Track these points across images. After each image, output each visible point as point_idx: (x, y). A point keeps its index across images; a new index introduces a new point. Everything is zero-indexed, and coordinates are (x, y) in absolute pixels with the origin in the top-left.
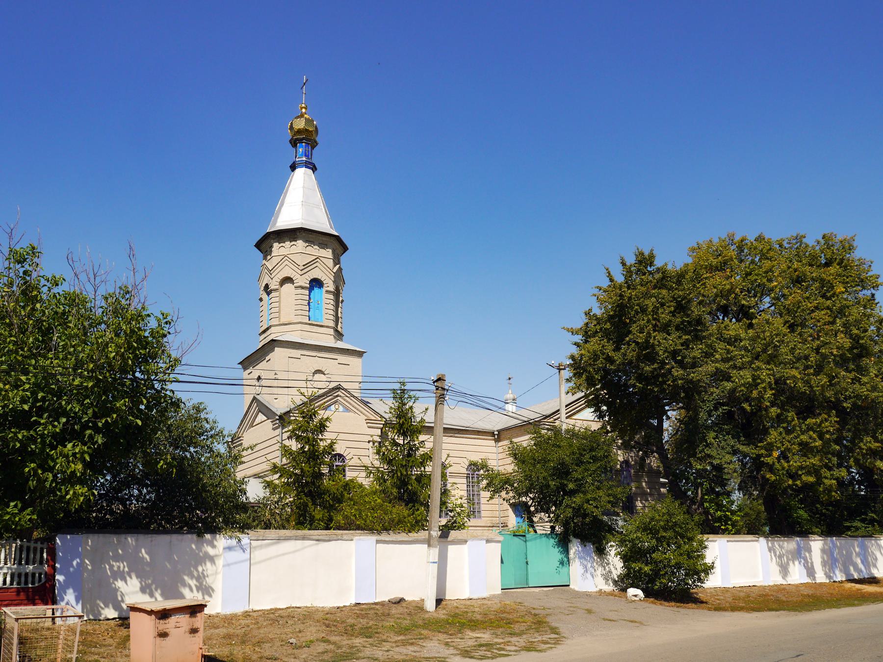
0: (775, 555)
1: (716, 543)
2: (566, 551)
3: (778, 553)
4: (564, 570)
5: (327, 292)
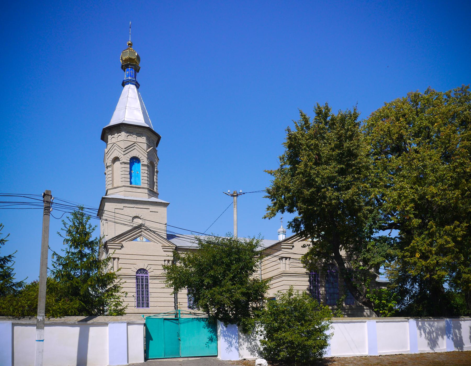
0: (425, 332)
1: (366, 324)
2: (215, 330)
3: (427, 330)
4: (213, 344)
5: (143, 165)
